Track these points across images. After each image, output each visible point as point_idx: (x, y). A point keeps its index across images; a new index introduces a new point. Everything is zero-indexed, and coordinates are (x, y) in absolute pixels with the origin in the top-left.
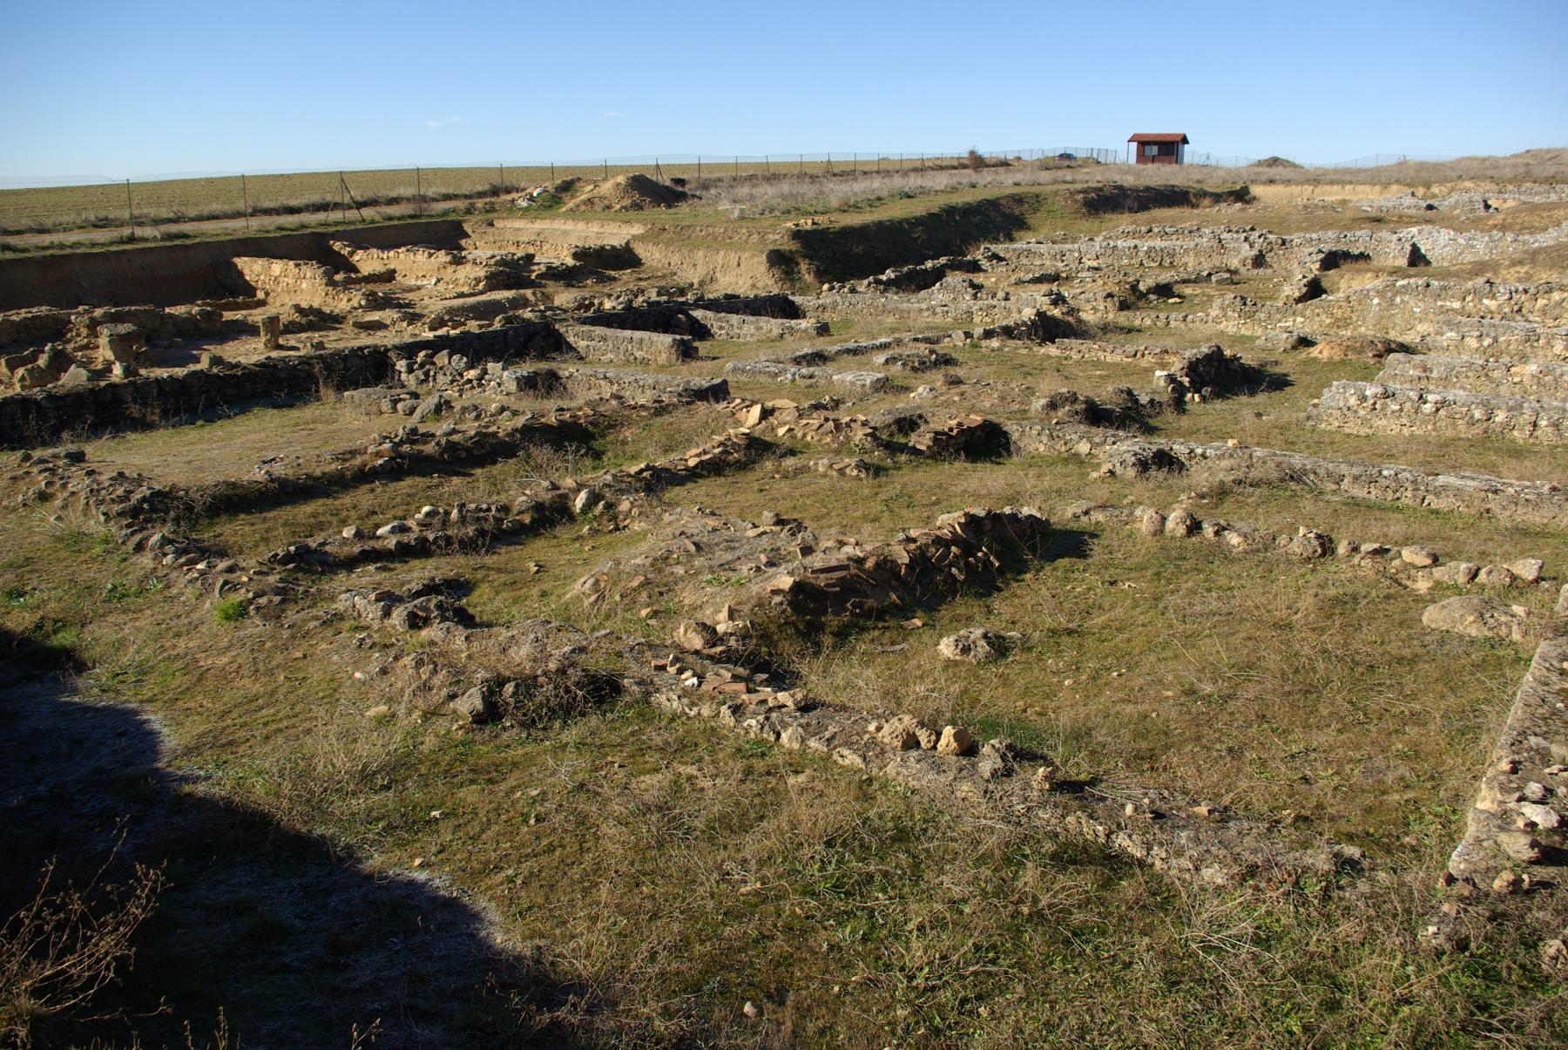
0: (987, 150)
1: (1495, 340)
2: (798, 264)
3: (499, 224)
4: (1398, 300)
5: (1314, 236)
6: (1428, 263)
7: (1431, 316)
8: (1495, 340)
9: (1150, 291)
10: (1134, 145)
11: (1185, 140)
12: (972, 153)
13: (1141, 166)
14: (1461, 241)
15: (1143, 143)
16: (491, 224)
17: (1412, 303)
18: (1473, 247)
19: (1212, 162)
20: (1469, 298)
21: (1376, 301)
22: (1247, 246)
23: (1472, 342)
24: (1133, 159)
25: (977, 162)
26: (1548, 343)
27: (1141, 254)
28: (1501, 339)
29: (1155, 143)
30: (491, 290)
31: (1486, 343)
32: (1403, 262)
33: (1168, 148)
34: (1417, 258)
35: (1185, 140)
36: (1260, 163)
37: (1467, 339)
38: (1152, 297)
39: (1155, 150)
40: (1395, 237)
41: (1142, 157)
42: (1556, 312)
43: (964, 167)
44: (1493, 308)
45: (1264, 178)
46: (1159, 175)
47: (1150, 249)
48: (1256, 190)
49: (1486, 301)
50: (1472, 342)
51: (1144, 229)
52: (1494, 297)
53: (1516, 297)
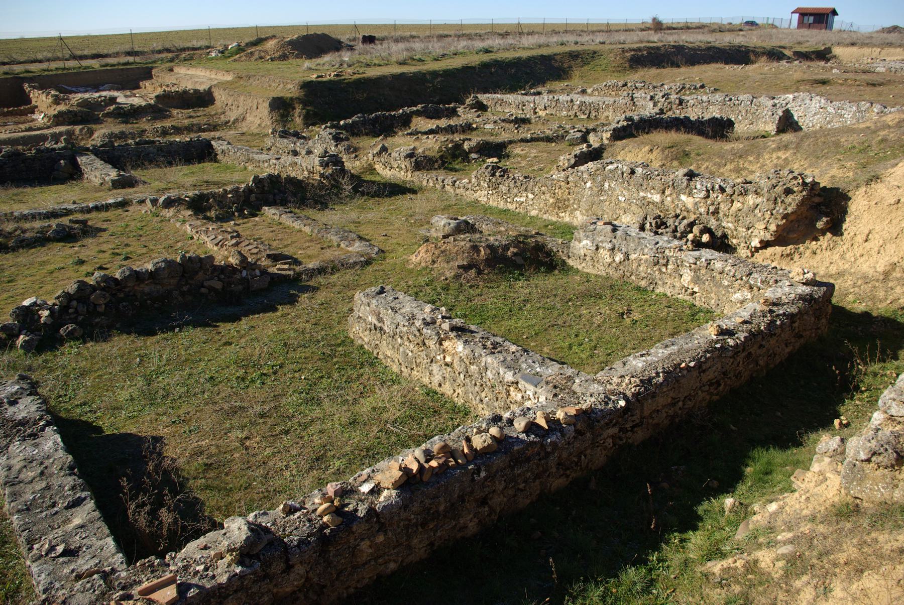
0: (666, 18)
1: (627, 257)
2: (294, 108)
3: (176, 70)
4: (606, 185)
5: (705, 98)
6: (800, 129)
7: (634, 208)
8: (627, 257)
9: (471, 150)
10: (796, 16)
11: (834, 12)
12: (654, 19)
13: (805, 32)
14: (831, 110)
15: (803, 14)
16: (171, 70)
17: (618, 192)
18: (841, 116)
19: (855, 28)
20: (667, 192)
21: (589, 184)
22: (651, 104)
23: (604, 254)
24: (795, 23)
25: (658, 26)
26: (676, 270)
27: (575, 107)
28: (633, 257)
29: (811, 14)
30: (57, 125)
31: (617, 259)
32: (771, 128)
33: (821, 18)
34: (787, 123)
35: (834, 12)
36: (883, 30)
37: (601, 251)
38: (473, 156)
39: (811, 19)
40: (771, 102)
41: (801, 24)
42: (748, 220)
43: (649, 29)
44: (690, 206)
45: (848, 41)
46: (814, 39)
47: (583, 103)
48: (837, 51)
49: (683, 197)
50: (604, 254)
51: (620, 84)
52: (690, 194)
53: (713, 195)
